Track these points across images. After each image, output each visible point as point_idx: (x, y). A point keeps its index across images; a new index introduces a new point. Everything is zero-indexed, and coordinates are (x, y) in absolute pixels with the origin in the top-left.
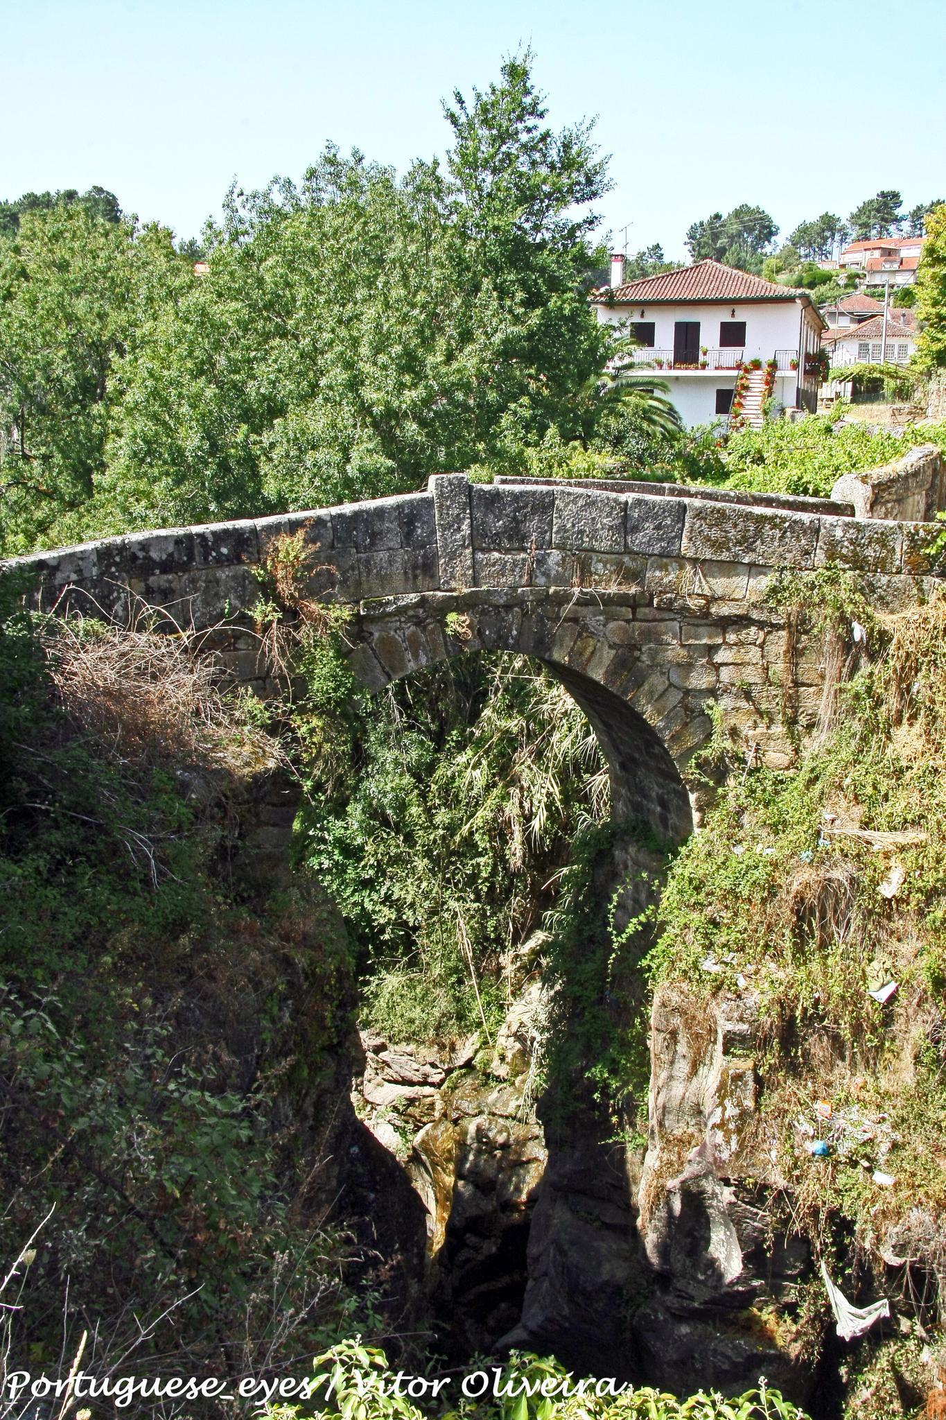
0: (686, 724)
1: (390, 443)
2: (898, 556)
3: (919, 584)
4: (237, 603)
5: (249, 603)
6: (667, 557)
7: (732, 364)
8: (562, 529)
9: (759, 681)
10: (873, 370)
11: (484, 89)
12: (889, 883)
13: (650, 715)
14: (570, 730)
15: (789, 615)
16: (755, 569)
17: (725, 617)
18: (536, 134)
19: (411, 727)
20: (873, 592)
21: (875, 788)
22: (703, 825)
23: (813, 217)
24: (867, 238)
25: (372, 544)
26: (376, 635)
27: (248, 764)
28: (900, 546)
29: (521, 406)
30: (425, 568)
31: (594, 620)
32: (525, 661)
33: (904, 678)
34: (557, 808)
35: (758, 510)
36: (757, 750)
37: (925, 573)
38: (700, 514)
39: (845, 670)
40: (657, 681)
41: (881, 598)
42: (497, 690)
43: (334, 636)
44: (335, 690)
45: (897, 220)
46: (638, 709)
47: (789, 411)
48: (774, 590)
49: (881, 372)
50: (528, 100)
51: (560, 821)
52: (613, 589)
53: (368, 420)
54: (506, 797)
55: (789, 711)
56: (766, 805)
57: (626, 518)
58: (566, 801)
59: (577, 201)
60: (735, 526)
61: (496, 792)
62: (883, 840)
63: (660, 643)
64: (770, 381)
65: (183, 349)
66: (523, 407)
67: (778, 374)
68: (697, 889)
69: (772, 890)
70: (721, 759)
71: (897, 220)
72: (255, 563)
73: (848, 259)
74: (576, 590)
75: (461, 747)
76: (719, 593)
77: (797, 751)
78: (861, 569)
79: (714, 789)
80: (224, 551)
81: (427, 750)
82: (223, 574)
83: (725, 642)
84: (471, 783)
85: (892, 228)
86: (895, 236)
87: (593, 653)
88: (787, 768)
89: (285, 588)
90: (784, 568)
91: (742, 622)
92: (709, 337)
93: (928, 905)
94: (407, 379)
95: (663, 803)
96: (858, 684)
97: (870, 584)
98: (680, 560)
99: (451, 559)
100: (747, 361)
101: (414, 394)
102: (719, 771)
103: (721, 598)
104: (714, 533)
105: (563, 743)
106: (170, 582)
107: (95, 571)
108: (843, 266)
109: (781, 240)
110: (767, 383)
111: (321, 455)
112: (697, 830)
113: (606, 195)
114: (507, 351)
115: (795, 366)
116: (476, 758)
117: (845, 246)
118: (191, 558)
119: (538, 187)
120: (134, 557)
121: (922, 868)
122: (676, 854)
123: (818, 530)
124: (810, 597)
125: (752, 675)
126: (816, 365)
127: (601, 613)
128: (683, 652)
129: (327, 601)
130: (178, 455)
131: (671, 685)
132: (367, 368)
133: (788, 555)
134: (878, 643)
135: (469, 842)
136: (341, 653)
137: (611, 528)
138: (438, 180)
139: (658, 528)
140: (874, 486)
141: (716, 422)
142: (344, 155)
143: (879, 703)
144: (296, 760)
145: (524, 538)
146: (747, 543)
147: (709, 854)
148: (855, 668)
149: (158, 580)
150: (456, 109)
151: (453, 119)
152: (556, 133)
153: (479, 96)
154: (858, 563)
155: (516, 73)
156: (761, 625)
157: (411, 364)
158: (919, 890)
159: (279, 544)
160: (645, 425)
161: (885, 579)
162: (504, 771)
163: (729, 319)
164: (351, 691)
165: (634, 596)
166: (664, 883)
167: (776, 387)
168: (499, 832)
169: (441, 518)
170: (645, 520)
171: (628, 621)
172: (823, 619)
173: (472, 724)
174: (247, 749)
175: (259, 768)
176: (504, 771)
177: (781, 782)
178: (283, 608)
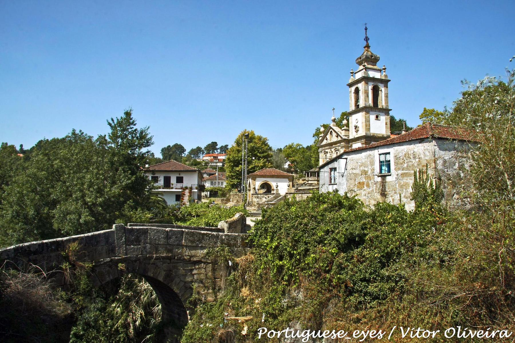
0: (185, 291)
1: (92, 213)
2: (239, 243)
3: (244, 250)
4: (57, 263)
5: (60, 263)
6: (179, 245)
7: (179, 187)
8: (150, 238)
9: (204, 278)
10: (216, 189)
11: (119, 118)
12: (244, 331)
13: (176, 290)
14: (146, 294)
15: (212, 260)
16: (202, 248)
17: (195, 261)
18: (133, 129)
19: (98, 297)
20: (233, 252)
21: (238, 305)
22: (191, 319)
23: (195, 147)
24: (209, 153)
25: (97, 244)
26: (98, 271)
27: (63, 312)
28: (239, 241)
29: (130, 202)
30: (112, 251)
31: (159, 264)
32: (132, 275)
33: (243, 275)
34: (143, 318)
35: (202, 232)
36: (205, 297)
37: (246, 247)
38: (187, 233)
39: (228, 274)
40: (177, 280)
41: (235, 254)
42: (124, 284)
43: (87, 272)
44: (87, 288)
45: (217, 149)
46: (172, 288)
47: (196, 201)
48: (208, 253)
49: (218, 189)
50: (131, 121)
51: (145, 322)
52: (164, 255)
53: (86, 206)
54: (128, 316)
55: (213, 286)
56: (209, 313)
57: (168, 235)
58: (146, 315)
59: (144, 147)
60: (197, 236)
61: (125, 314)
62: (241, 319)
63: (178, 269)
64: (191, 192)
65: (28, 185)
66: (130, 202)
67: (193, 191)
68: (191, 338)
69: (213, 336)
70: (195, 300)
71: (217, 149)
72: (62, 251)
73: (205, 158)
74: (155, 255)
75: (113, 302)
76: (193, 255)
77: (216, 297)
78: (230, 246)
79: (194, 309)
80: (53, 247)
81: (103, 303)
82: (53, 254)
83: (195, 268)
84: (117, 312)
85: (215, 151)
86: (216, 153)
87: (159, 273)
88: (213, 302)
89: (73, 258)
90: (210, 247)
91: (199, 262)
92: (173, 180)
93: (255, 336)
94: (98, 195)
95: (179, 314)
96: (231, 277)
97: (232, 251)
98: (183, 246)
99: (119, 248)
100: (184, 187)
101: (101, 199)
102: (195, 304)
103: (194, 256)
104: (191, 238)
105: (144, 298)
106: (36, 257)
107: (13, 255)
108: (203, 160)
109: (186, 153)
110: (190, 193)
111: (73, 217)
112: (190, 321)
113: (152, 146)
114: (127, 187)
115: (196, 189)
116: (118, 305)
117: (203, 155)
118: (43, 250)
119: (134, 143)
120: (26, 250)
121: (252, 326)
122: (184, 329)
123: (218, 237)
124: (218, 254)
125: (202, 277)
126: (201, 188)
127: (161, 261)
128: (184, 271)
129: (84, 261)
130: (26, 217)
131: (181, 281)
132: (87, 192)
133: (211, 244)
134: (235, 266)
135: (117, 330)
136: (89, 277)
137: (164, 238)
138: (106, 140)
139: (176, 237)
140: (229, 224)
141: (176, 204)
142: (77, 132)
143: (237, 282)
144: (75, 310)
145: (140, 241)
146: (200, 241)
147: (194, 328)
148: (230, 273)
149: (32, 257)
150: (111, 122)
151: (110, 124)
152: (139, 129)
153: (118, 120)
154: (229, 245)
155: (128, 114)
156: (205, 263)
157: (100, 191)
158: (252, 332)
159: (70, 245)
160: (157, 205)
161: (236, 249)
162: (127, 309)
163: (179, 176)
164: (92, 288)
165: (170, 256)
166: (181, 337)
167: (192, 194)
168: (126, 326)
169: (116, 237)
170: (173, 235)
171: (169, 264)
172: (221, 262)
173: (116, 295)
174: (62, 308)
175: (66, 313)
176: (127, 309)
177: (212, 306)
178: (70, 264)
